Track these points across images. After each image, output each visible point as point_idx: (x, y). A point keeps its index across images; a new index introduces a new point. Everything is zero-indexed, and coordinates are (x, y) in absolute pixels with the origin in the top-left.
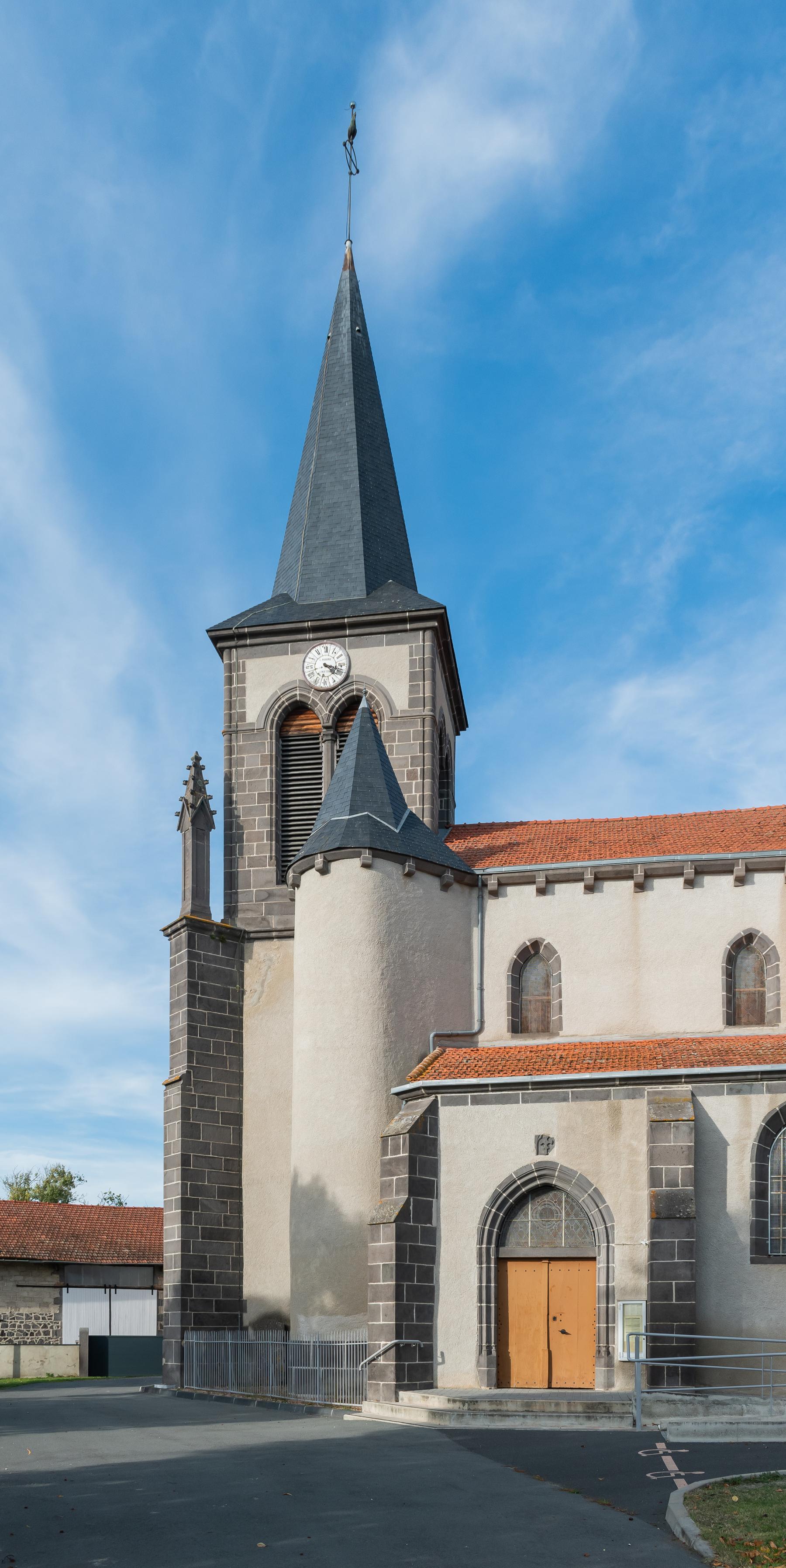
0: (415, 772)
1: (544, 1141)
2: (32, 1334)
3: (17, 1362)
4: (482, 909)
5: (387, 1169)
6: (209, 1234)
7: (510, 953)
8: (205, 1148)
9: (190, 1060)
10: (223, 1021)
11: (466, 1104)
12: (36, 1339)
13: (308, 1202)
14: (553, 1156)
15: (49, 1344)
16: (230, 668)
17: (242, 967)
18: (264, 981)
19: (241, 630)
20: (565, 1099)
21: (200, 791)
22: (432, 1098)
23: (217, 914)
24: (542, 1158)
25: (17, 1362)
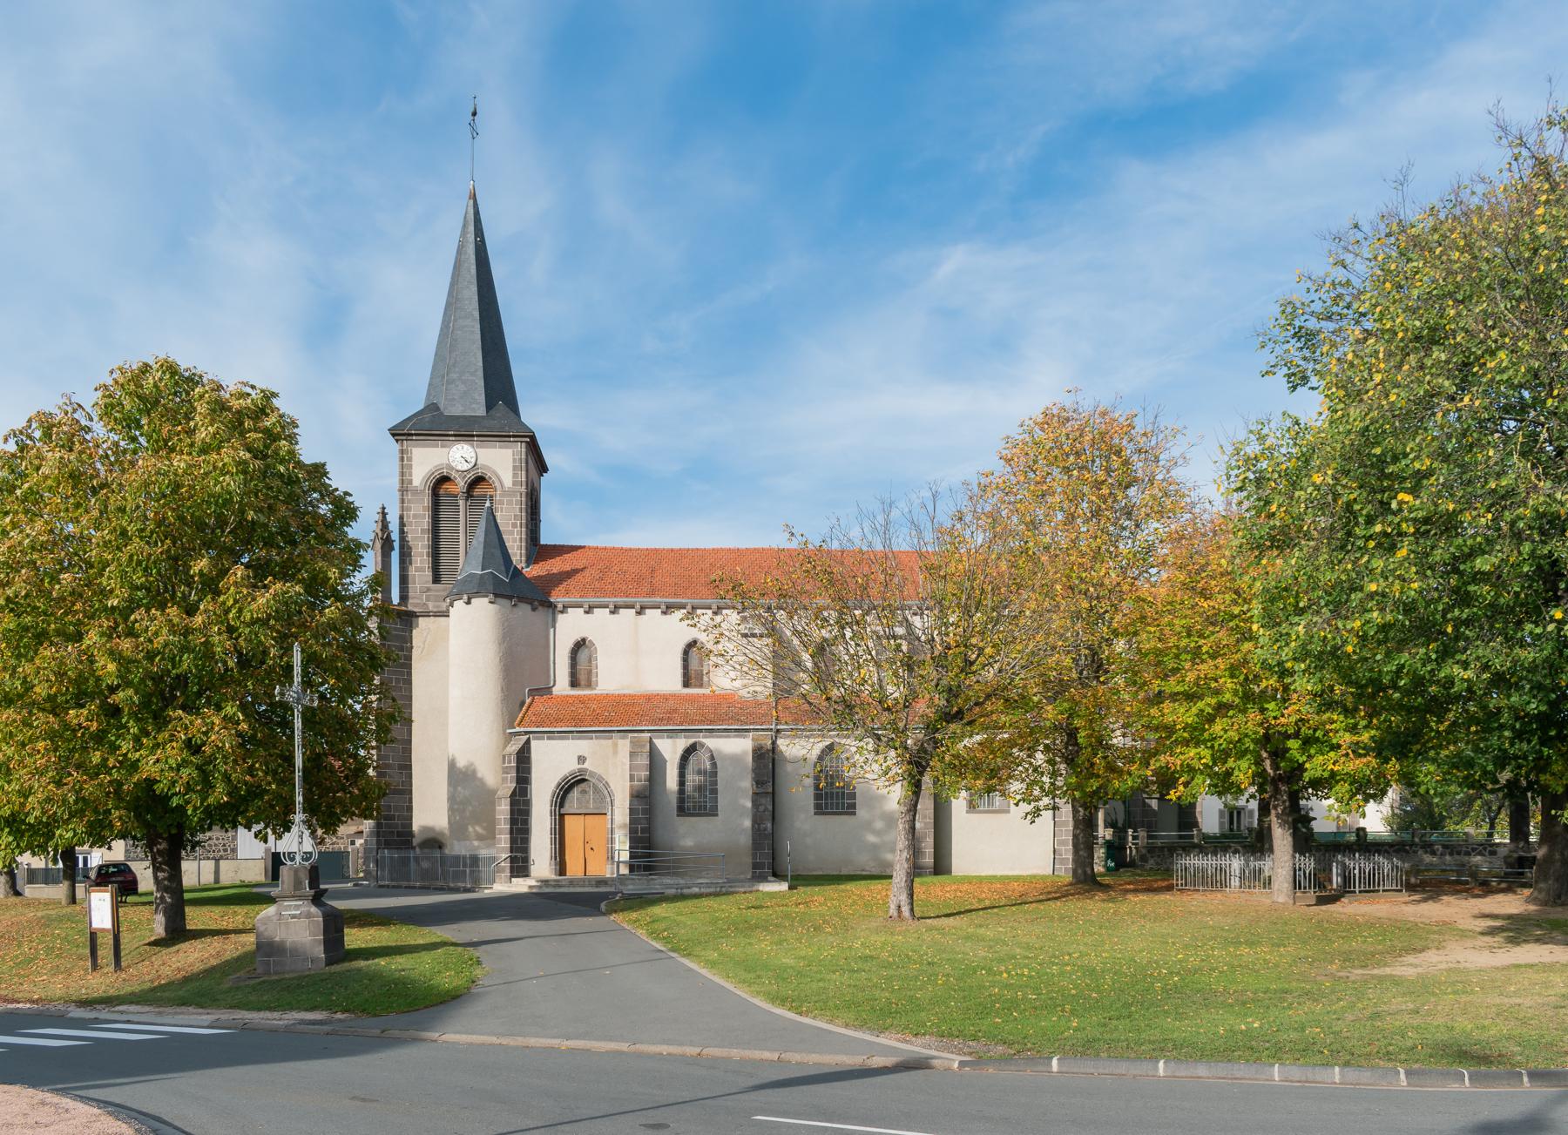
3: (217, 872)
4: (554, 621)
5: (506, 771)
7: (570, 645)
13: (459, 777)
16: (402, 452)
23: (396, 599)
25: (217, 872)
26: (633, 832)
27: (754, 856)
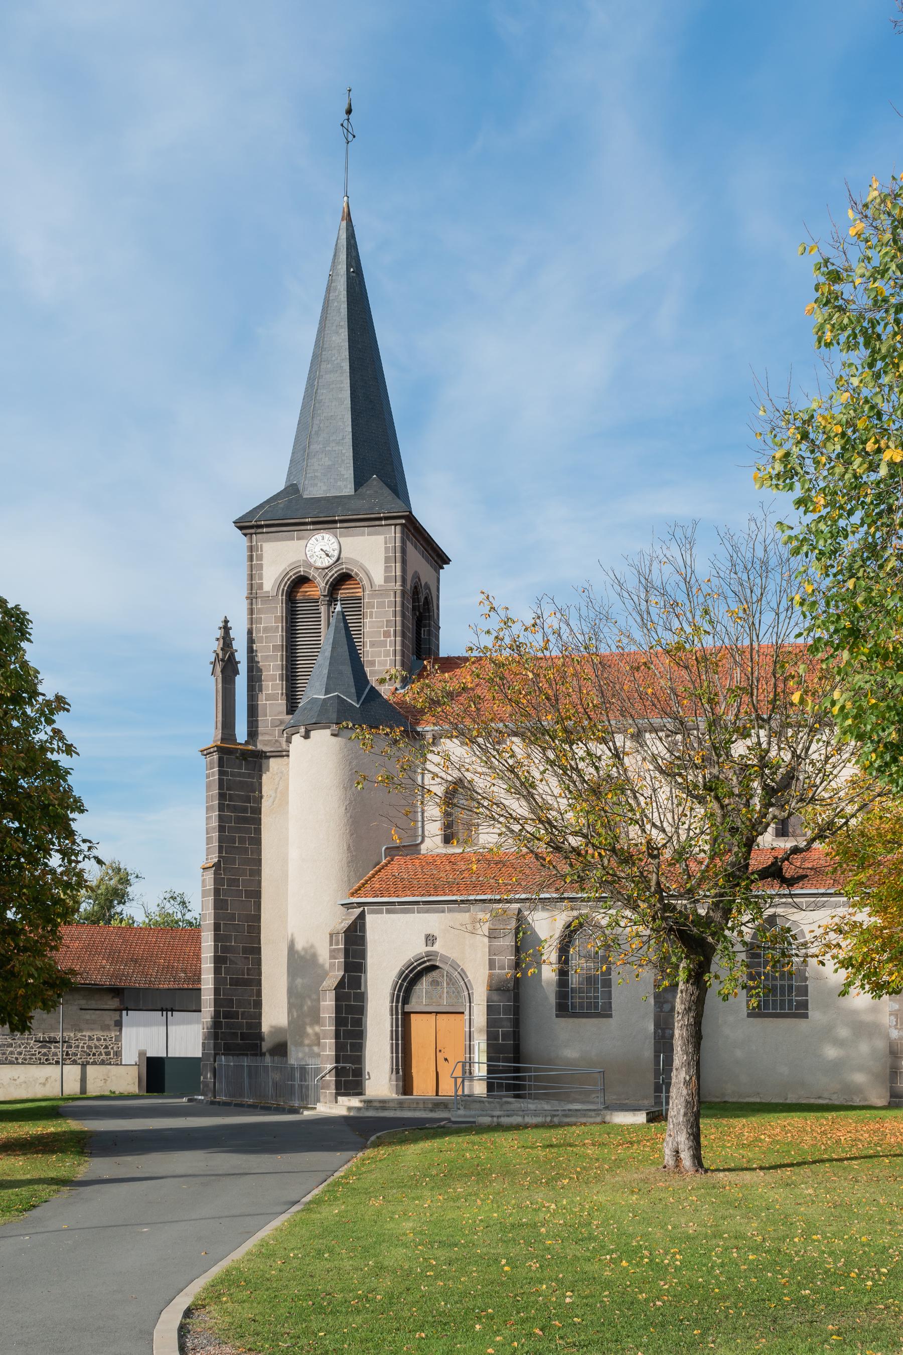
0: (389, 632)
1: (430, 937)
2: (94, 1055)
8: (233, 917)
9: (220, 852)
10: (246, 820)
11: (382, 913)
13: (300, 963)
14: (436, 947)
15: (110, 1064)
16: (251, 549)
17: (261, 778)
18: (277, 789)
19: (259, 523)
20: (443, 912)
21: (228, 646)
22: (361, 909)
23: (241, 733)
24: (429, 949)
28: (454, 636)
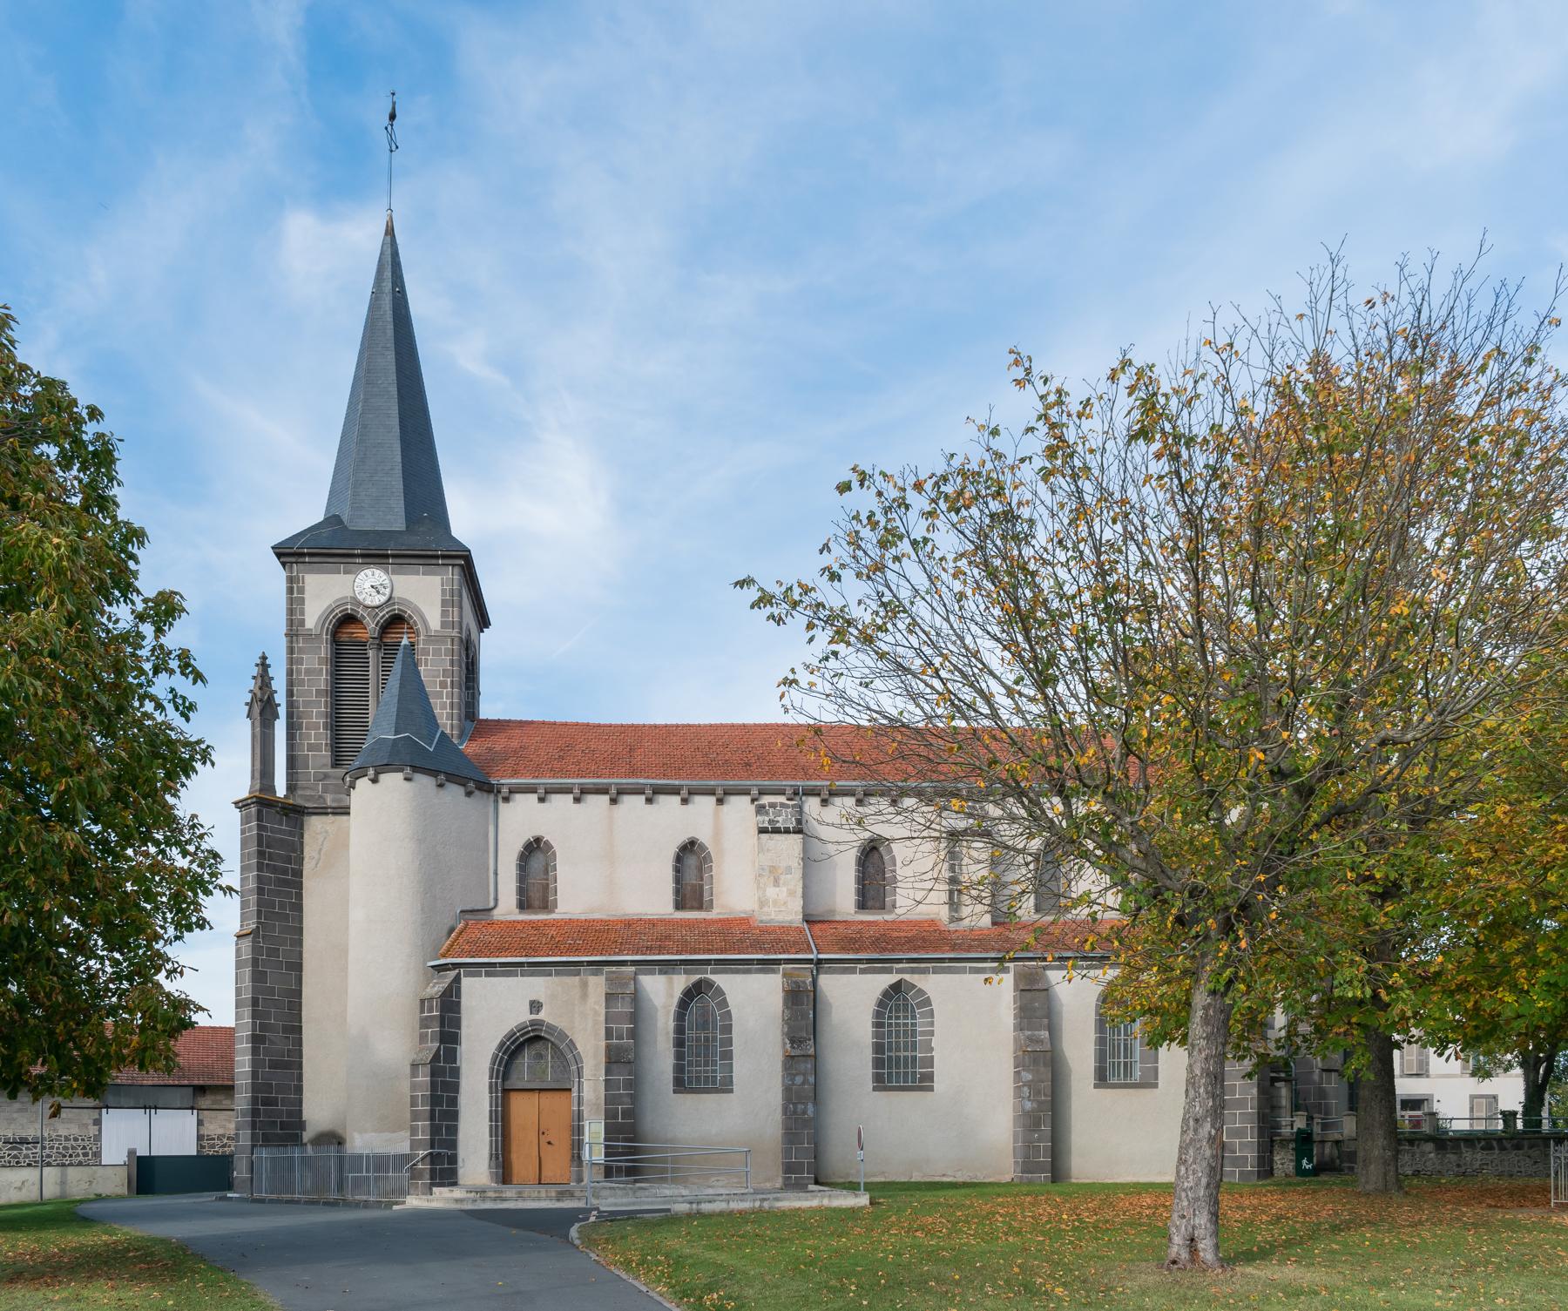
5: (424, 1023)
6: (274, 1065)
7: (518, 847)
8: (271, 991)
10: (286, 883)
12: (75, 1160)
16: (290, 580)
17: (302, 836)
23: (281, 790)
24: (534, 1017)
25: (63, 1183)
26: (610, 1115)
27: (787, 1153)
28: (488, 710)
